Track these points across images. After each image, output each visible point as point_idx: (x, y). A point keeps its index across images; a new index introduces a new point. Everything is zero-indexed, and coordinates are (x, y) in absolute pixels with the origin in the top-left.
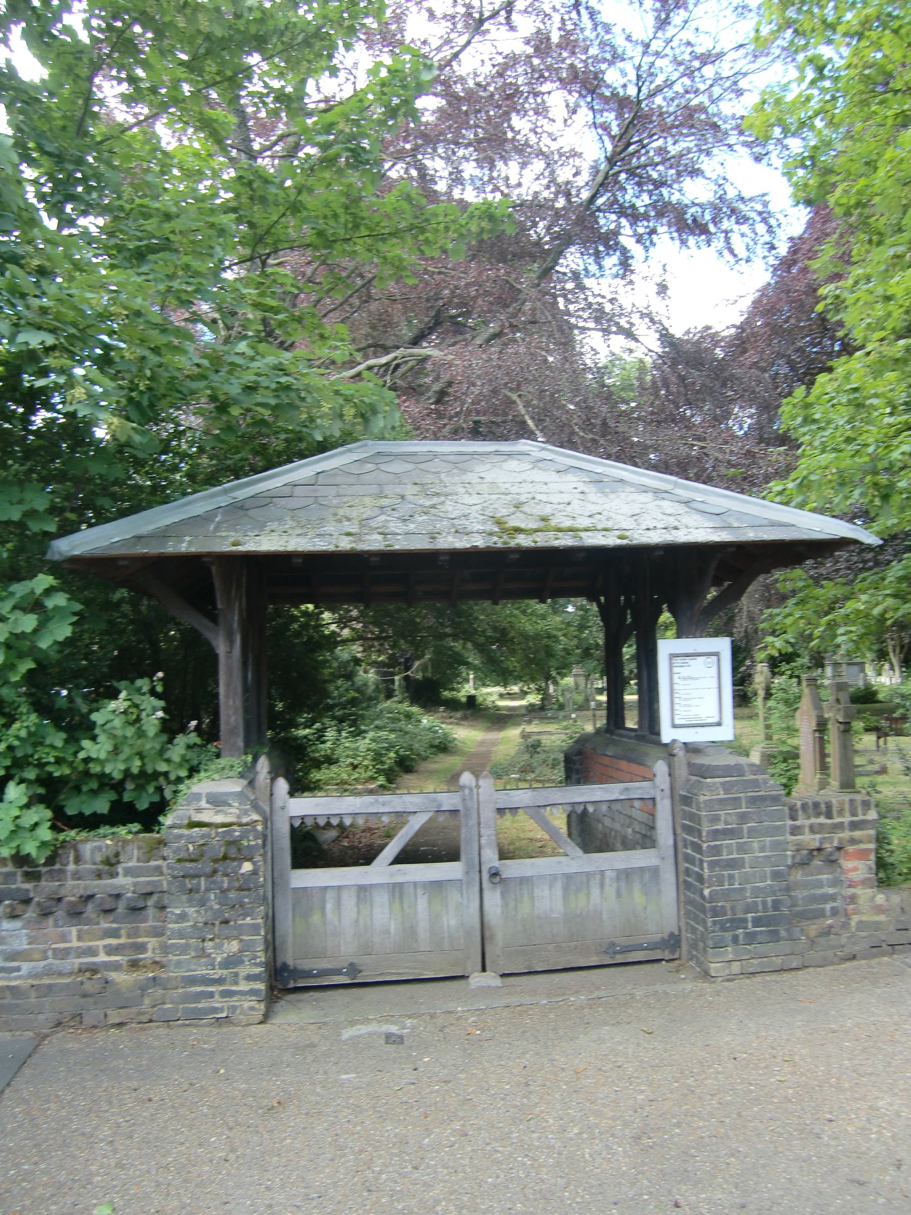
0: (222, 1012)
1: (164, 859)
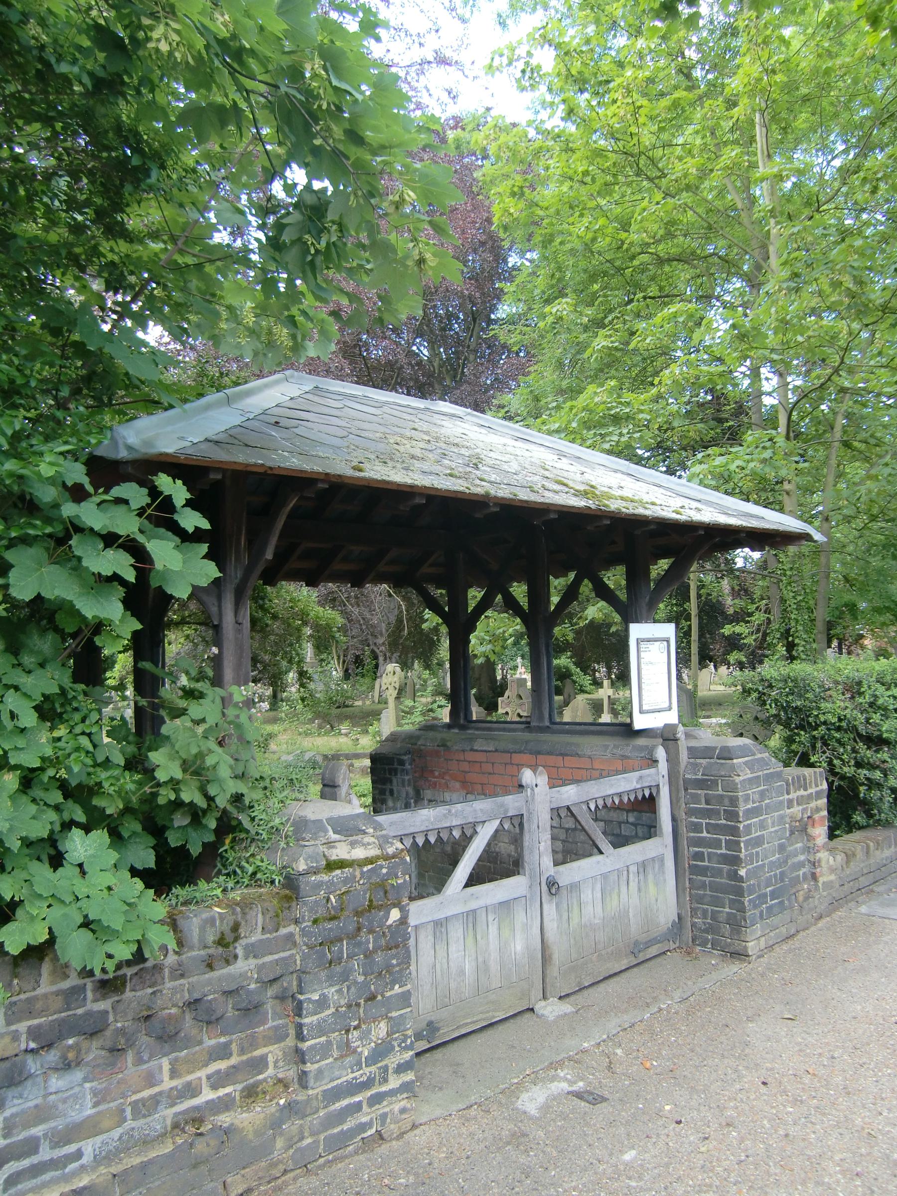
0: (370, 1128)
1: (297, 922)
